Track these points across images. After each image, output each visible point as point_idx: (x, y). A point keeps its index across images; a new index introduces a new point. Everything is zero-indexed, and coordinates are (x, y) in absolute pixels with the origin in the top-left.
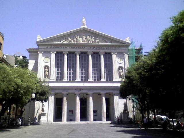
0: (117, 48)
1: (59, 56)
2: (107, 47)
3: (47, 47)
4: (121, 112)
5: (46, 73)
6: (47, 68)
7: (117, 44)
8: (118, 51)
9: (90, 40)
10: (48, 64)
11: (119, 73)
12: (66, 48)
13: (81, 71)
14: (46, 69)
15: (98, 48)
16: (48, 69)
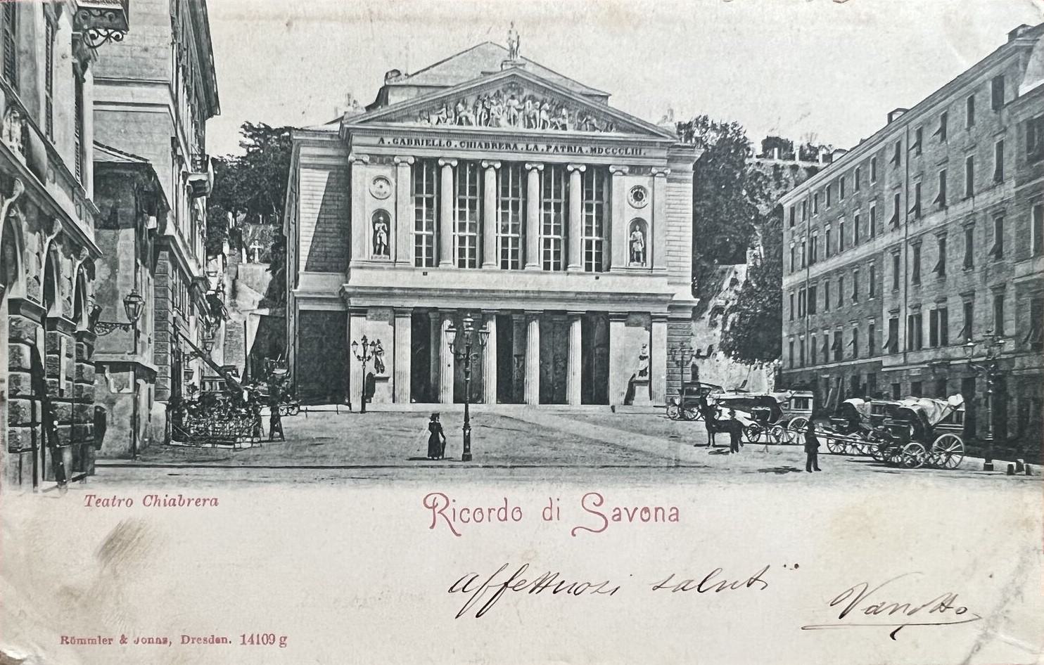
0: (629, 150)
1: (425, 170)
2: (597, 146)
3: (382, 140)
4: (121, 522)
5: (381, 238)
6: (381, 218)
7: (632, 137)
8: (634, 162)
9: (534, 117)
10: (388, 206)
11: (631, 243)
12: (449, 143)
13: (500, 208)
14: (379, 222)
15: (563, 148)
16: (387, 222)
